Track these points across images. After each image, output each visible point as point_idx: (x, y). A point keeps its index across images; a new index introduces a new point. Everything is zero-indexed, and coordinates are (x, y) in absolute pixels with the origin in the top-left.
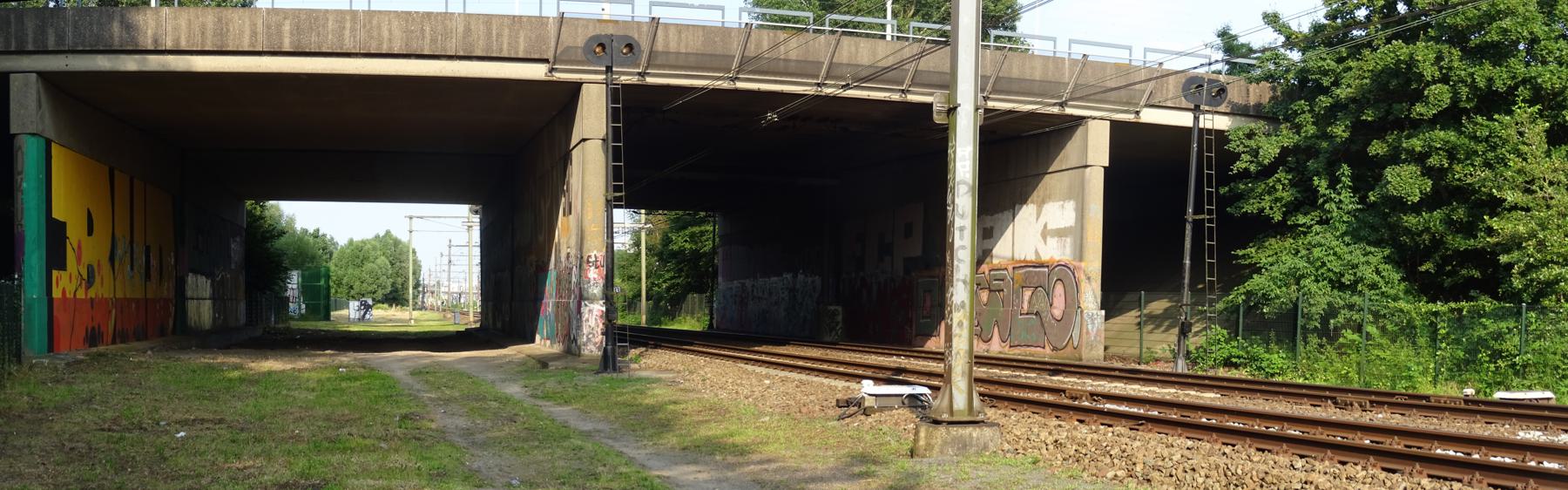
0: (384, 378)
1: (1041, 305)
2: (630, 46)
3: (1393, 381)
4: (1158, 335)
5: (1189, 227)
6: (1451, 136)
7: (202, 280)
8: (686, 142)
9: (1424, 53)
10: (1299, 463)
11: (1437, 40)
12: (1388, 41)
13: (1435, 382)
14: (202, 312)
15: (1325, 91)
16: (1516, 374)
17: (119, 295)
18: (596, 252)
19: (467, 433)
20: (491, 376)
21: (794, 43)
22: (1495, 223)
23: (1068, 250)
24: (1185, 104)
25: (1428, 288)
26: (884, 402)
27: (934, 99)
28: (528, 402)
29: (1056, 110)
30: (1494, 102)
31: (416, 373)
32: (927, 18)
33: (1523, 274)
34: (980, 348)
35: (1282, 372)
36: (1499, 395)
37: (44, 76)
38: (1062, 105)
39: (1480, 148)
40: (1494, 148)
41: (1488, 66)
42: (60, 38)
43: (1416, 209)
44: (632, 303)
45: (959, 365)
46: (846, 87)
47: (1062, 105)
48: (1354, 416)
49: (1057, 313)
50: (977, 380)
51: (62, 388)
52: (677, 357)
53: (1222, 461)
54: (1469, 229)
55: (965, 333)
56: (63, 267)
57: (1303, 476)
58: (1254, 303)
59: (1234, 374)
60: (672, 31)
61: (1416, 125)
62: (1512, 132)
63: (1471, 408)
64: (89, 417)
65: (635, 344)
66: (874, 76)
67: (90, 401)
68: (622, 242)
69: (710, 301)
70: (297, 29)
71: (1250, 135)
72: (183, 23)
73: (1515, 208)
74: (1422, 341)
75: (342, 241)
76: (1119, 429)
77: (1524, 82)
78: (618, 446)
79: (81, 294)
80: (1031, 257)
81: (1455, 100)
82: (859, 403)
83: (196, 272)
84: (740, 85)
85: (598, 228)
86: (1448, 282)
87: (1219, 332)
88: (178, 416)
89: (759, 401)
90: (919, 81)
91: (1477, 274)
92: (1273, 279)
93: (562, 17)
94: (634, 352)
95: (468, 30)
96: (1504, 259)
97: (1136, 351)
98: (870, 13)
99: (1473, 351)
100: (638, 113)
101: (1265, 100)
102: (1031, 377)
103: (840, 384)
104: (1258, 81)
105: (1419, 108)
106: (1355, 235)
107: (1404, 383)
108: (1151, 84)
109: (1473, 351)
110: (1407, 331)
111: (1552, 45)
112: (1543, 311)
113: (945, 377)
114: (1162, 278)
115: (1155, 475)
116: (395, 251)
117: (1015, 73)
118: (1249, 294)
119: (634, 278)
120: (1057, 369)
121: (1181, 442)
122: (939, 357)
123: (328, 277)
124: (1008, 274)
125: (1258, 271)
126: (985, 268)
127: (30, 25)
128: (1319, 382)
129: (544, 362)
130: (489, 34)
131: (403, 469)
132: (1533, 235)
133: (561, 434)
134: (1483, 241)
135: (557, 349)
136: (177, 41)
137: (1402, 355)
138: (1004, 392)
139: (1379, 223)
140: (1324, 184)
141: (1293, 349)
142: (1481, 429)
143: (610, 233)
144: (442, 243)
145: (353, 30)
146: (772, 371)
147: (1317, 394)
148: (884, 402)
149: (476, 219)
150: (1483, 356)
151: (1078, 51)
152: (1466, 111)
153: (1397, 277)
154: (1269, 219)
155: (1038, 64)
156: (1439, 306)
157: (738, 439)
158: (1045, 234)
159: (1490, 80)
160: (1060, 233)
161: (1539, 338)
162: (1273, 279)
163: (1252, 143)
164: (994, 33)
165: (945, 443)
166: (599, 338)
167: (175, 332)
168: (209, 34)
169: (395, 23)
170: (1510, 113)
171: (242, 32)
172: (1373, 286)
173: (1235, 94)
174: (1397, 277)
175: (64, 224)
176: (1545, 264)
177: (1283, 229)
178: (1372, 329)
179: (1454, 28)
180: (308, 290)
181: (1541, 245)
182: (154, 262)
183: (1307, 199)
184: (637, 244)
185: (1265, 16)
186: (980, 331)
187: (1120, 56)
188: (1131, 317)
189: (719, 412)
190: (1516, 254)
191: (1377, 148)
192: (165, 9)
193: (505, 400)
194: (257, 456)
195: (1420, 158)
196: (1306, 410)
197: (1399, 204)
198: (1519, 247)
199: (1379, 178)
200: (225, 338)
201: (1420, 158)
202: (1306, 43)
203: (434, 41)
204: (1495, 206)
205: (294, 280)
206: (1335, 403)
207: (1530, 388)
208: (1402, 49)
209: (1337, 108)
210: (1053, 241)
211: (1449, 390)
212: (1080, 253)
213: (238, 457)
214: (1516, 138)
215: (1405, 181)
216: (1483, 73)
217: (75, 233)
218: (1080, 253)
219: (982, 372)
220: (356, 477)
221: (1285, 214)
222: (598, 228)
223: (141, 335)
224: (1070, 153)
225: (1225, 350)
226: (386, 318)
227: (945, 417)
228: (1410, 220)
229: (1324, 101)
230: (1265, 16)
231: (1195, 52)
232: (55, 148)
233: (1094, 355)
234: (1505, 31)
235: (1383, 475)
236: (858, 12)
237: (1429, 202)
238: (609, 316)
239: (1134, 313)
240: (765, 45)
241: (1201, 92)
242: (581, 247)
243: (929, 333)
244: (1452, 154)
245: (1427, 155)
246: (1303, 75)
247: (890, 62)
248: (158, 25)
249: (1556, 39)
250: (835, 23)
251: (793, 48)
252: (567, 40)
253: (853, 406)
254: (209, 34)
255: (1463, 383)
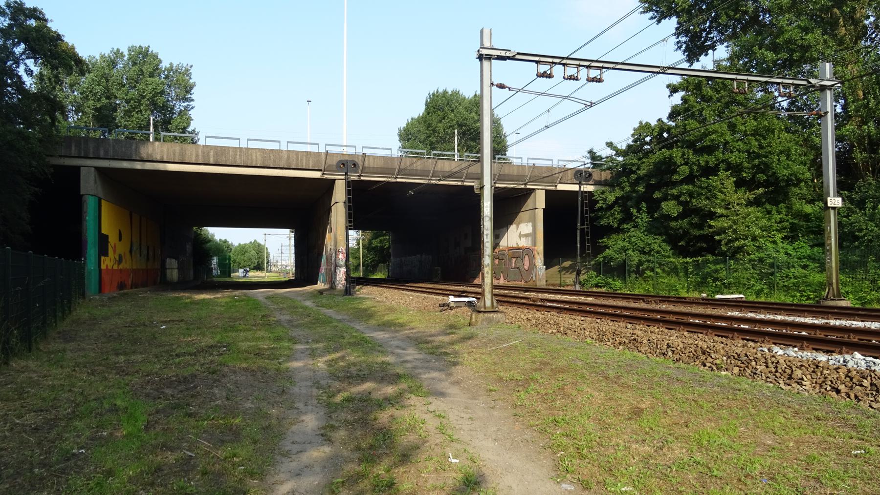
0: (254, 300)
1: (519, 265)
2: (354, 165)
3: (669, 291)
4: (567, 275)
5: (578, 231)
6: (691, 187)
7: (173, 261)
8: (377, 201)
9: (676, 153)
10: (629, 326)
11: (682, 147)
12: (660, 149)
13: (688, 292)
14: (173, 274)
15: (634, 172)
16: (726, 287)
17: (134, 267)
18: (342, 248)
19: (290, 322)
20: (299, 298)
21: (419, 162)
22: (712, 223)
23: (530, 242)
24: (575, 181)
25: (682, 252)
26: (458, 304)
27: (474, 184)
28: (315, 308)
29: (523, 187)
30: (709, 171)
31: (268, 298)
32: (471, 152)
33: (726, 244)
34: (496, 282)
35: (620, 289)
36: (717, 297)
37: (98, 169)
38: (525, 184)
39: (704, 192)
40: (710, 191)
41: (706, 156)
42: (106, 152)
43: (676, 219)
44: (357, 268)
45: (487, 288)
46: (440, 180)
47: (525, 184)
48: (652, 306)
49: (526, 267)
50: (495, 295)
51: (106, 309)
52: (375, 288)
53: (596, 325)
54: (700, 226)
55: (490, 276)
56: (106, 254)
57: (631, 331)
58: (607, 261)
59: (600, 290)
60: (371, 159)
61: (674, 184)
62: (718, 183)
63: (705, 302)
64: (119, 321)
65: (358, 284)
66: (451, 175)
67: (119, 314)
68: (352, 244)
69: (388, 266)
70: (216, 154)
71: (603, 193)
72: (165, 150)
73: (721, 216)
74: (681, 274)
75: (236, 244)
76: (553, 313)
77: (723, 161)
78: (352, 325)
79: (115, 267)
80: (515, 246)
81: (691, 172)
82: (448, 305)
83: (171, 257)
84: (398, 180)
85: (342, 237)
86: (691, 249)
87: (593, 273)
88: (162, 319)
89: (408, 307)
90: (469, 177)
91: (705, 245)
92: (615, 251)
93: (327, 153)
94: (358, 287)
95: (289, 157)
96: (717, 238)
97: (558, 282)
98: (448, 150)
99: (705, 278)
100: (356, 190)
101: (608, 178)
102: (516, 293)
103: (440, 298)
104: (605, 170)
105: (675, 177)
106: (649, 231)
107: (674, 292)
108: (561, 174)
109: (705, 278)
110: (674, 270)
111: (735, 144)
112: (737, 260)
113: (482, 294)
114: (569, 253)
115: (569, 331)
116: (259, 249)
117: (506, 172)
118: (605, 257)
119: (358, 258)
120: (527, 290)
121: (579, 318)
122: (479, 286)
123: (230, 259)
124: (506, 253)
125: (608, 248)
126: (496, 250)
127: (91, 146)
128: (636, 293)
129: (321, 292)
130: (297, 159)
131: (263, 338)
132: (730, 227)
133: (328, 321)
134: (707, 231)
135: (327, 286)
136: (162, 157)
137: (673, 281)
138: (506, 299)
139: (659, 225)
140: (635, 211)
141: (624, 280)
142: (710, 311)
143: (348, 240)
144: (278, 245)
145: (240, 156)
146: (413, 293)
147: (636, 298)
148: (458, 304)
149: (293, 235)
150: (709, 280)
151: (531, 162)
152: (696, 176)
153: (668, 248)
154: (612, 226)
155: (515, 169)
156: (688, 260)
157: (400, 321)
158: (520, 236)
159: (707, 162)
160: (526, 236)
161: (735, 271)
162: (615, 251)
163: (604, 196)
164: (497, 157)
165: (483, 320)
166: (344, 282)
167: (161, 283)
168: (177, 155)
169: (259, 153)
170: (717, 175)
171: (192, 154)
172: (658, 252)
173: (596, 176)
174: (668, 248)
175: (107, 236)
176: (737, 239)
177: (618, 231)
178: (659, 270)
179: (689, 141)
180: (221, 265)
181: (735, 231)
182: (151, 253)
183: (628, 218)
184: (358, 244)
185: (607, 143)
186: (495, 276)
187: (548, 163)
188: (556, 269)
189: (392, 310)
190: (723, 236)
191: (657, 195)
192: (157, 143)
193: (305, 308)
194: (198, 335)
195: (676, 198)
196: (631, 304)
197: (668, 218)
198: (724, 232)
199: (658, 207)
200: (184, 285)
201: (676, 198)
202: (624, 153)
203: (274, 161)
204: (712, 215)
205: (215, 260)
206: (644, 301)
207: (732, 293)
208: (666, 152)
209: (639, 179)
210: (523, 239)
211: (695, 295)
212: (534, 243)
213: (190, 335)
214: (720, 186)
215: (670, 207)
216: (703, 159)
217: (113, 240)
218: (534, 243)
219: (496, 291)
220: (242, 341)
221: (619, 224)
222: (342, 237)
223: (144, 285)
224: (529, 204)
225: (598, 280)
226: (255, 276)
227: (483, 309)
228: (673, 224)
229: (634, 176)
230: (607, 143)
231: (578, 159)
232: (103, 202)
233: (542, 284)
234: (713, 140)
235: (667, 331)
236: (444, 150)
237: (681, 216)
238: (347, 273)
239: (557, 267)
240: (408, 164)
241: (581, 176)
242: (336, 245)
243: (475, 276)
244: (691, 194)
245: (680, 196)
246: (624, 166)
247: (457, 169)
248: (153, 150)
249: (737, 141)
250: (435, 155)
251: (419, 165)
252: (329, 162)
253: (445, 306)
254: (177, 155)
255: (702, 292)
